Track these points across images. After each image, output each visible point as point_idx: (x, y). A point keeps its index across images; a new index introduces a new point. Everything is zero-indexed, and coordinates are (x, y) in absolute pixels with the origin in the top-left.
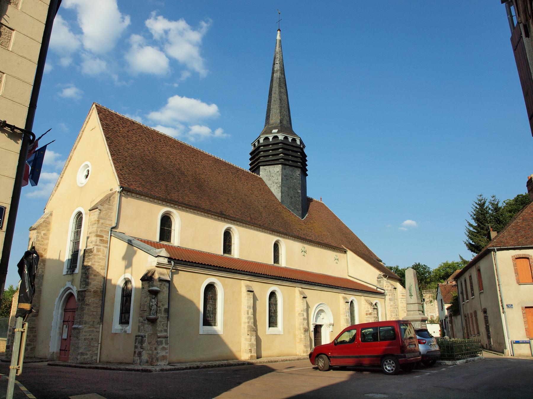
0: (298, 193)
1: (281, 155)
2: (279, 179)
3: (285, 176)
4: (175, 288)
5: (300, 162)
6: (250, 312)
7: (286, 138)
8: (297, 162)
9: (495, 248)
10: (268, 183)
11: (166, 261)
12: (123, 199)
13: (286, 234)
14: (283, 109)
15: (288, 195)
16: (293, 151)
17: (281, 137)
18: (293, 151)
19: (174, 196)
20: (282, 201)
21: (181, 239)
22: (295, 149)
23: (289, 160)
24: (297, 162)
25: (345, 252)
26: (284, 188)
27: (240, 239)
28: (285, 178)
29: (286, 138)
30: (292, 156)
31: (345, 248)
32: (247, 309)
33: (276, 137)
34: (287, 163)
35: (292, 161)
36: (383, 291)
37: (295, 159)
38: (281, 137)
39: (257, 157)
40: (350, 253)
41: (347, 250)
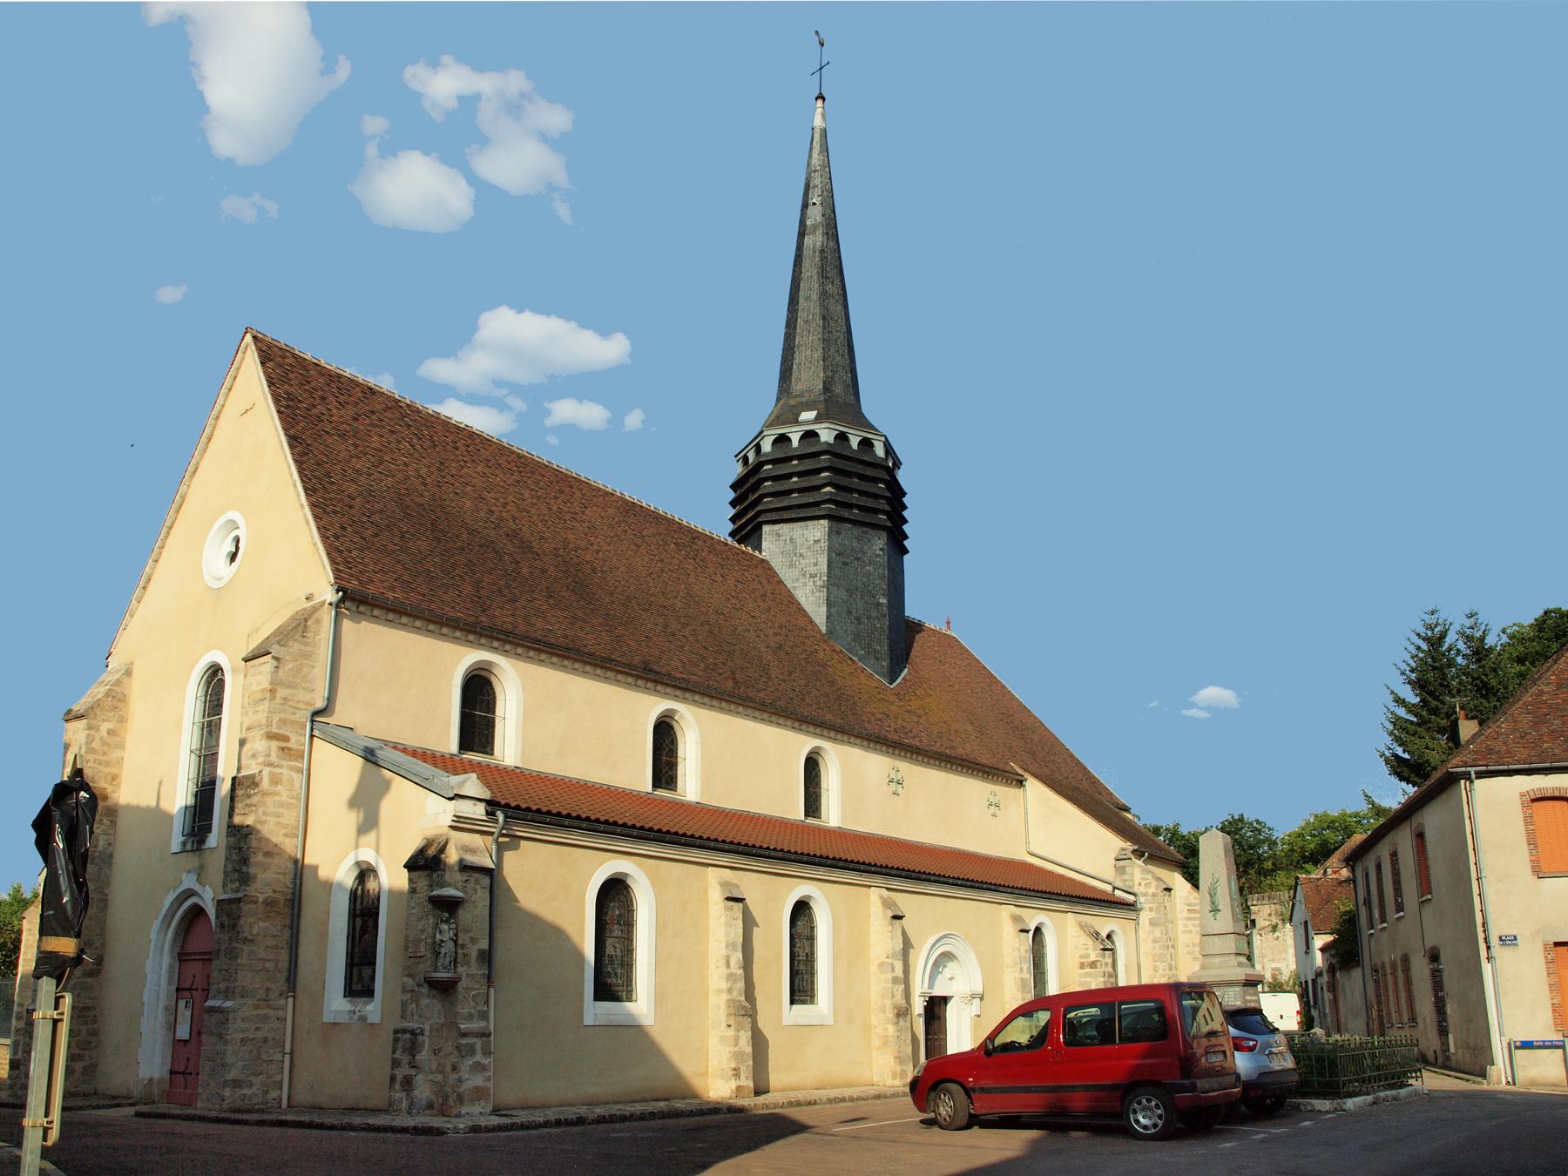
0: (879, 604)
1: (828, 489)
3: (839, 554)
5: (883, 512)
6: (733, 962)
7: (842, 437)
8: (876, 511)
10: (787, 576)
12: (347, 624)
14: (833, 348)
15: (849, 613)
16: (862, 477)
17: (826, 435)
18: (862, 477)
20: (830, 631)
22: (870, 472)
24: (876, 511)
25: (1020, 783)
26: (835, 590)
28: (839, 560)
29: (782, 439)
30: (861, 493)
31: (1020, 771)
32: (724, 952)
33: (810, 435)
34: (845, 514)
36: (1131, 898)
37: (870, 503)
38: (826, 435)
39: (752, 498)
40: (1033, 786)
41: (1027, 775)
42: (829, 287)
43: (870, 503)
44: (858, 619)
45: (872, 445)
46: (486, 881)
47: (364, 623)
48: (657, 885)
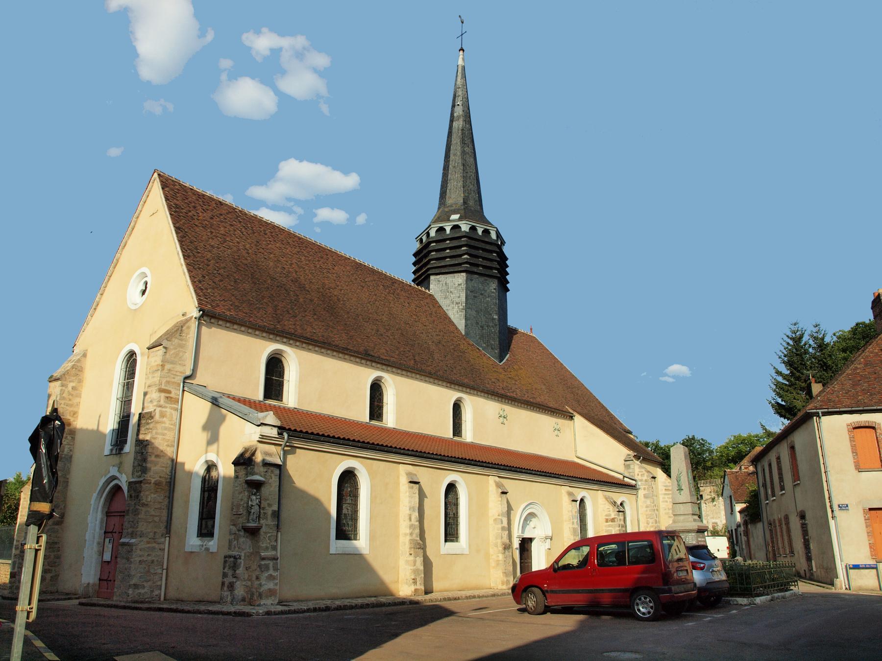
1: (466, 256)
2: (461, 296)
3: (471, 292)
4: (290, 476)
7: (473, 228)
8: (491, 268)
9: (820, 411)
10: (444, 303)
11: (274, 432)
12: (204, 329)
13: (473, 388)
14: (468, 181)
15: (477, 323)
17: (465, 227)
19: (289, 325)
20: (467, 333)
21: (300, 396)
22: (488, 247)
23: (477, 265)
24: (491, 268)
25: (571, 418)
26: (469, 311)
27: (398, 395)
28: (472, 295)
29: (473, 228)
30: (484, 258)
31: (571, 411)
32: (408, 512)
33: (456, 227)
35: (484, 267)
36: (633, 482)
37: (488, 264)
38: (465, 227)
40: (579, 419)
41: (575, 413)
42: (466, 149)
43: (488, 264)
44: (482, 327)
45: (489, 233)
46: (277, 472)
47: (214, 329)
48: (372, 475)
